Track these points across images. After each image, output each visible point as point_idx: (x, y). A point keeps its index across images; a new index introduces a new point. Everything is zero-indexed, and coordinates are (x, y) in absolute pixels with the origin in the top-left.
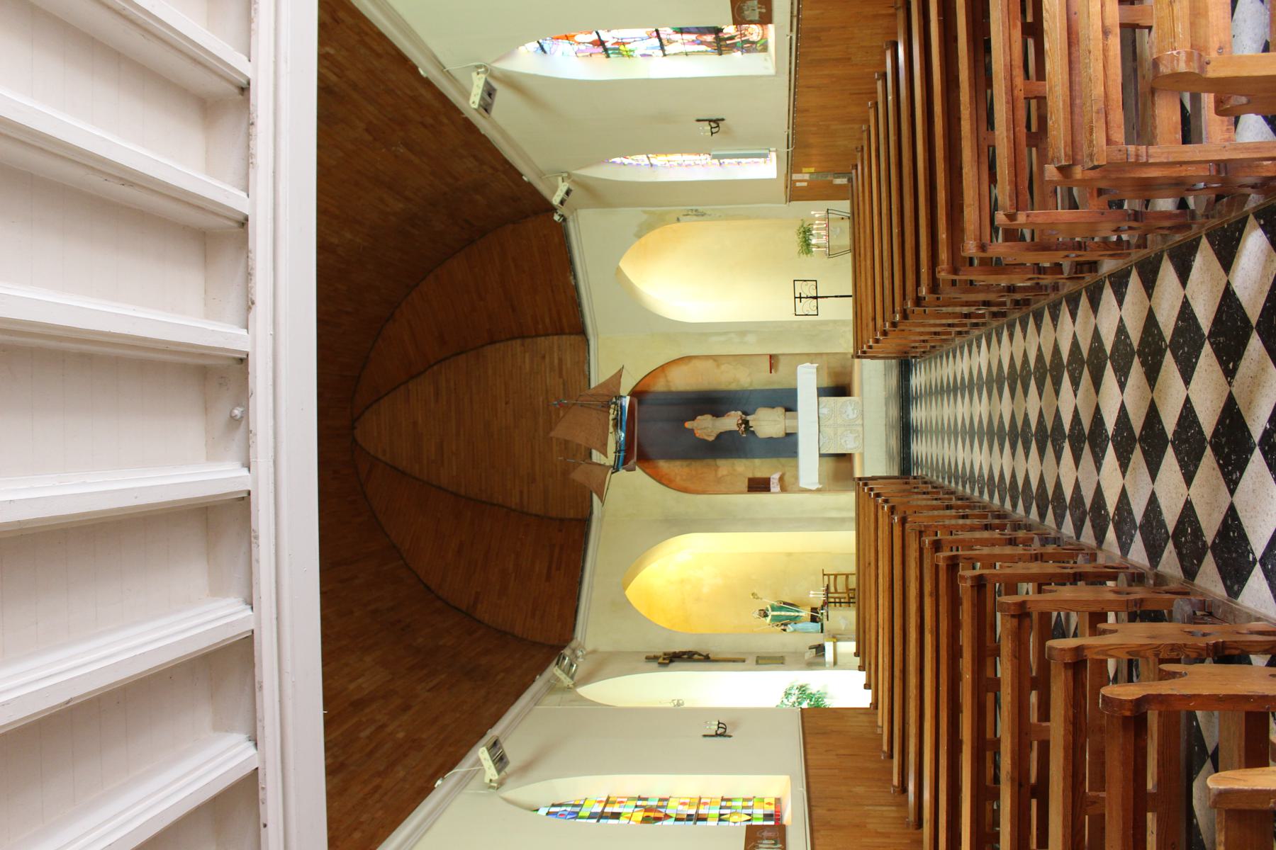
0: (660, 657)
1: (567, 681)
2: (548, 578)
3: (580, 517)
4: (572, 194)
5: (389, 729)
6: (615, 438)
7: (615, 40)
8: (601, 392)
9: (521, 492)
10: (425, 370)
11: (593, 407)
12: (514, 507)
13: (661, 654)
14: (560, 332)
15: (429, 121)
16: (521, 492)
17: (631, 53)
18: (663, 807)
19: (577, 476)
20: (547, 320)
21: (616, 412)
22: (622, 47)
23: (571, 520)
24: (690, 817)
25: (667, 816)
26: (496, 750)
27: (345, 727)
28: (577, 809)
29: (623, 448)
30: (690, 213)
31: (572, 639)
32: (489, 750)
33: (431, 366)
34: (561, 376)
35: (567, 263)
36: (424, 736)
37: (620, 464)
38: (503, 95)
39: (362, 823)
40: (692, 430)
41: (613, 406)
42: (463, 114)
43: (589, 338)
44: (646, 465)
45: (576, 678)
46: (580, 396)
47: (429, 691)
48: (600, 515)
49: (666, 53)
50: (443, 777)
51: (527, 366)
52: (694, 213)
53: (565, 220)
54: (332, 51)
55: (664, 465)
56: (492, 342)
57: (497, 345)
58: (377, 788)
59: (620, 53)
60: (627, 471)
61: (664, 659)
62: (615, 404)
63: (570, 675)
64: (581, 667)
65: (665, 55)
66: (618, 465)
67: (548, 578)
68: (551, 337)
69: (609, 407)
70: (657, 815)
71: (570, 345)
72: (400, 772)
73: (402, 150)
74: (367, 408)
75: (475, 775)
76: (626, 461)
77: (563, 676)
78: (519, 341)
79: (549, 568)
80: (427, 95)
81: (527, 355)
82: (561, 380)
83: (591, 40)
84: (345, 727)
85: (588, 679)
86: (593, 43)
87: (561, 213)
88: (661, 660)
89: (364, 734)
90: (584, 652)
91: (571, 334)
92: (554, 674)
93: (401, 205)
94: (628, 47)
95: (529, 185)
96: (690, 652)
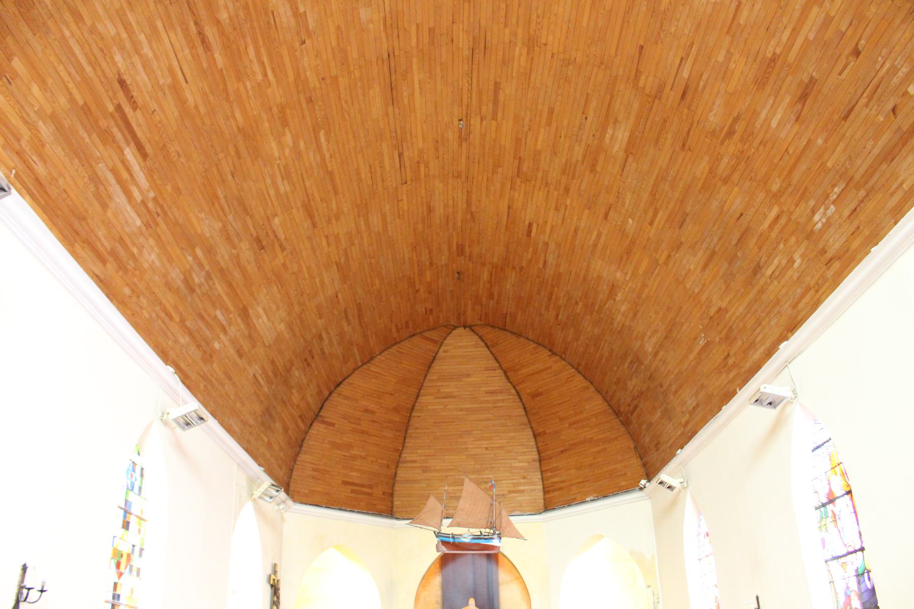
0: (276, 577)
1: (257, 493)
2: (346, 483)
3: (395, 509)
4: (668, 491)
5: (222, 336)
6: (466, 534)
7: (837, 513)
8: (503, 520)
9: (415, 462)
10: (511, 383)
11: (491, 514)
12: (403, 455)
13: (278, 578)
14: (546, 491)
15: (731, 361)
16: (415, 462)
17: (823, 529)
18: (131, 571)
19: (432, 502)
20: (555, 480)
21: (487, 534)
22: (830, 520)
24: (116, 597)
25: (120, 575)
26: (196, 420)
27: (225, 298)
28: (136, 489)
29: (456, 540)
30: (656, 597)
31: (294, 500)
32: (195, 411)
33: (514, 387)
34: (510, 492)
35: (604, 494)
36: (215, 366)
37: (443, 538)
38: (768, 414)
39: (138, 297)
40: (467, 604)
41: (492, 531)
42: (740, 389)
44: (438, 565)
45: (260, 501)
46: (500, 503)
47: (254, 375)
49: (829, 563)
50: (176, 373)
51: (517, 465)
52: (656, 600)
53: (641, 489)
54: (796, 265)
55: (437, 580)
56: (535, 436)
57: (533, 440)
58: (171, 318)
59: (822, 518)
60: (437, 545)
61: (274, 580)
62: (494, 534)
63: (263, 496)
64: (270, 507)
65: (826, 562)
66: (441, 536)
67: (346, 483)
68: (541, 483)
69: (491, 528)
70: (123, 566)
71: (536, 500)
72: (184, 339)
73: (702, 343)
74: (481, 338)
75: (176, 402)
76: (445, 543)
77: (262, 489)
78: (537, 457)
79: (353, 484)
80: (756, 355)
81: (526, 464)
82: (506, 492)
83: (834, 490)
84: (225, 298)
85: (260, 512)
86: (831, 493)
87: (646, 486)
88: (273, 577)
89: (218, 313)
90: (282, 511)
91: (545, 499)
92: (263, 482)
93: (650, 350)
94: (831, 526)
95: (673, 455)
96: (279, 602)
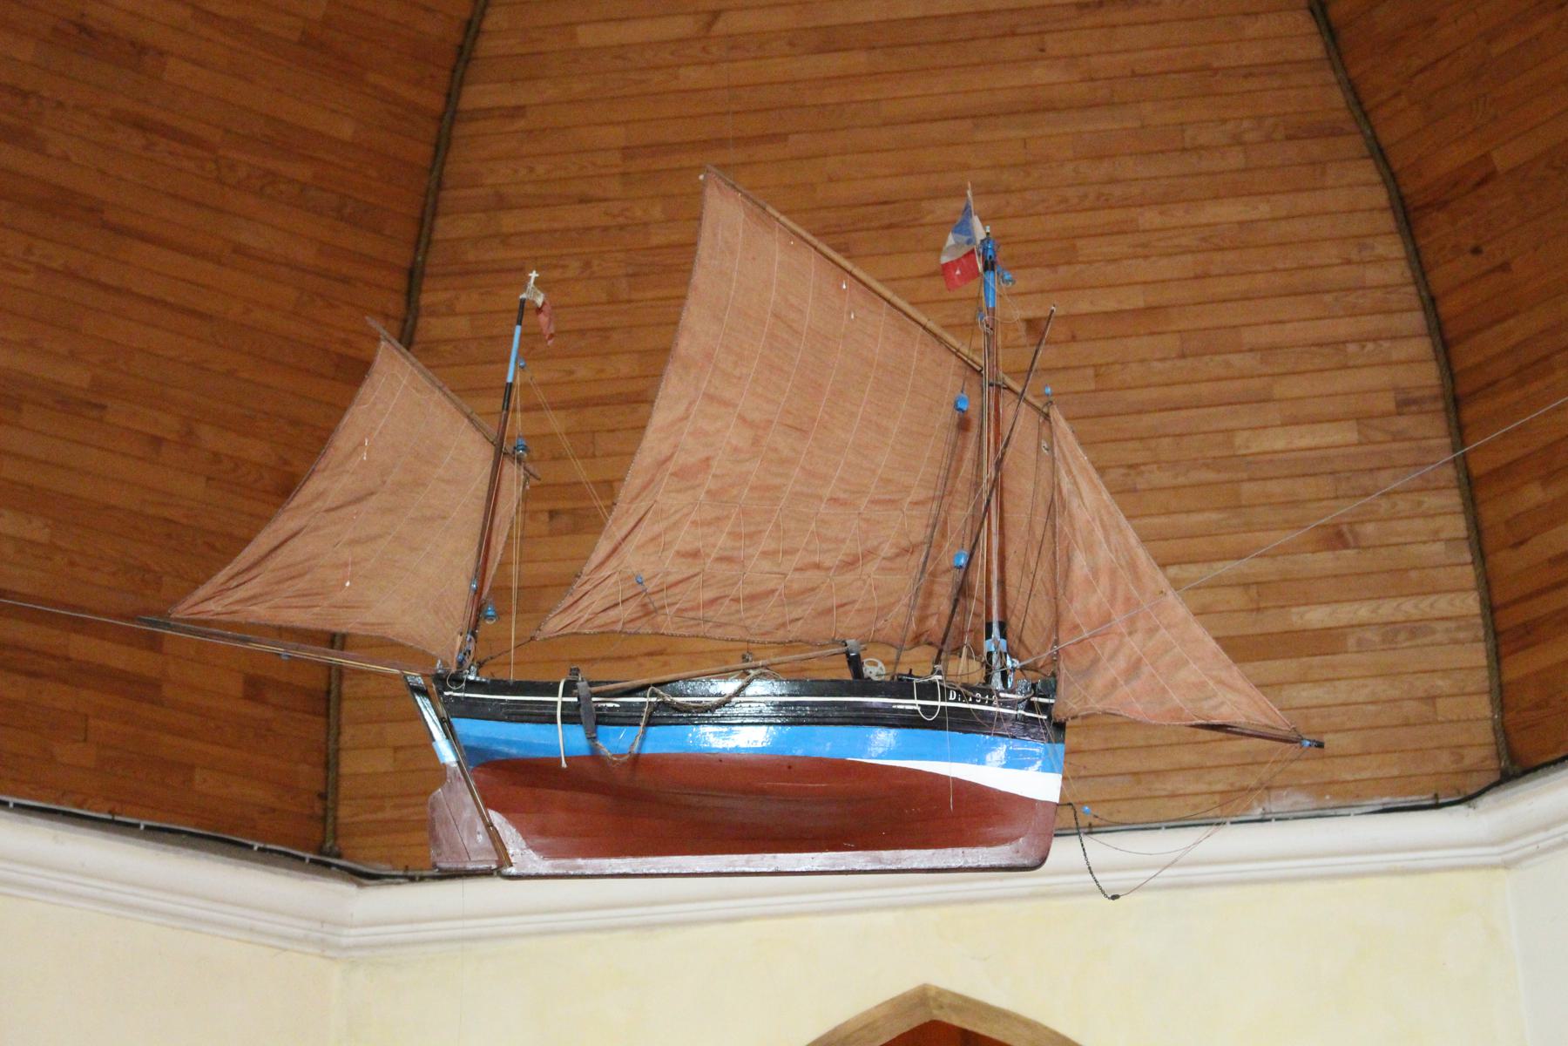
23: (329, 762)
43: (1487, 801)
48: (350, 936)
51: (1278, 441)
57: (1393, 248)
71: (1431, 699)
78: (1428, 376)
81: (1344, 434)
91: (1502, 695)
